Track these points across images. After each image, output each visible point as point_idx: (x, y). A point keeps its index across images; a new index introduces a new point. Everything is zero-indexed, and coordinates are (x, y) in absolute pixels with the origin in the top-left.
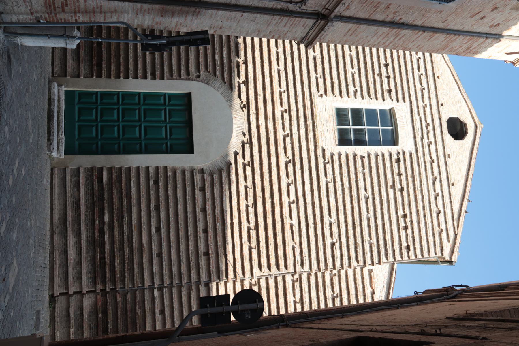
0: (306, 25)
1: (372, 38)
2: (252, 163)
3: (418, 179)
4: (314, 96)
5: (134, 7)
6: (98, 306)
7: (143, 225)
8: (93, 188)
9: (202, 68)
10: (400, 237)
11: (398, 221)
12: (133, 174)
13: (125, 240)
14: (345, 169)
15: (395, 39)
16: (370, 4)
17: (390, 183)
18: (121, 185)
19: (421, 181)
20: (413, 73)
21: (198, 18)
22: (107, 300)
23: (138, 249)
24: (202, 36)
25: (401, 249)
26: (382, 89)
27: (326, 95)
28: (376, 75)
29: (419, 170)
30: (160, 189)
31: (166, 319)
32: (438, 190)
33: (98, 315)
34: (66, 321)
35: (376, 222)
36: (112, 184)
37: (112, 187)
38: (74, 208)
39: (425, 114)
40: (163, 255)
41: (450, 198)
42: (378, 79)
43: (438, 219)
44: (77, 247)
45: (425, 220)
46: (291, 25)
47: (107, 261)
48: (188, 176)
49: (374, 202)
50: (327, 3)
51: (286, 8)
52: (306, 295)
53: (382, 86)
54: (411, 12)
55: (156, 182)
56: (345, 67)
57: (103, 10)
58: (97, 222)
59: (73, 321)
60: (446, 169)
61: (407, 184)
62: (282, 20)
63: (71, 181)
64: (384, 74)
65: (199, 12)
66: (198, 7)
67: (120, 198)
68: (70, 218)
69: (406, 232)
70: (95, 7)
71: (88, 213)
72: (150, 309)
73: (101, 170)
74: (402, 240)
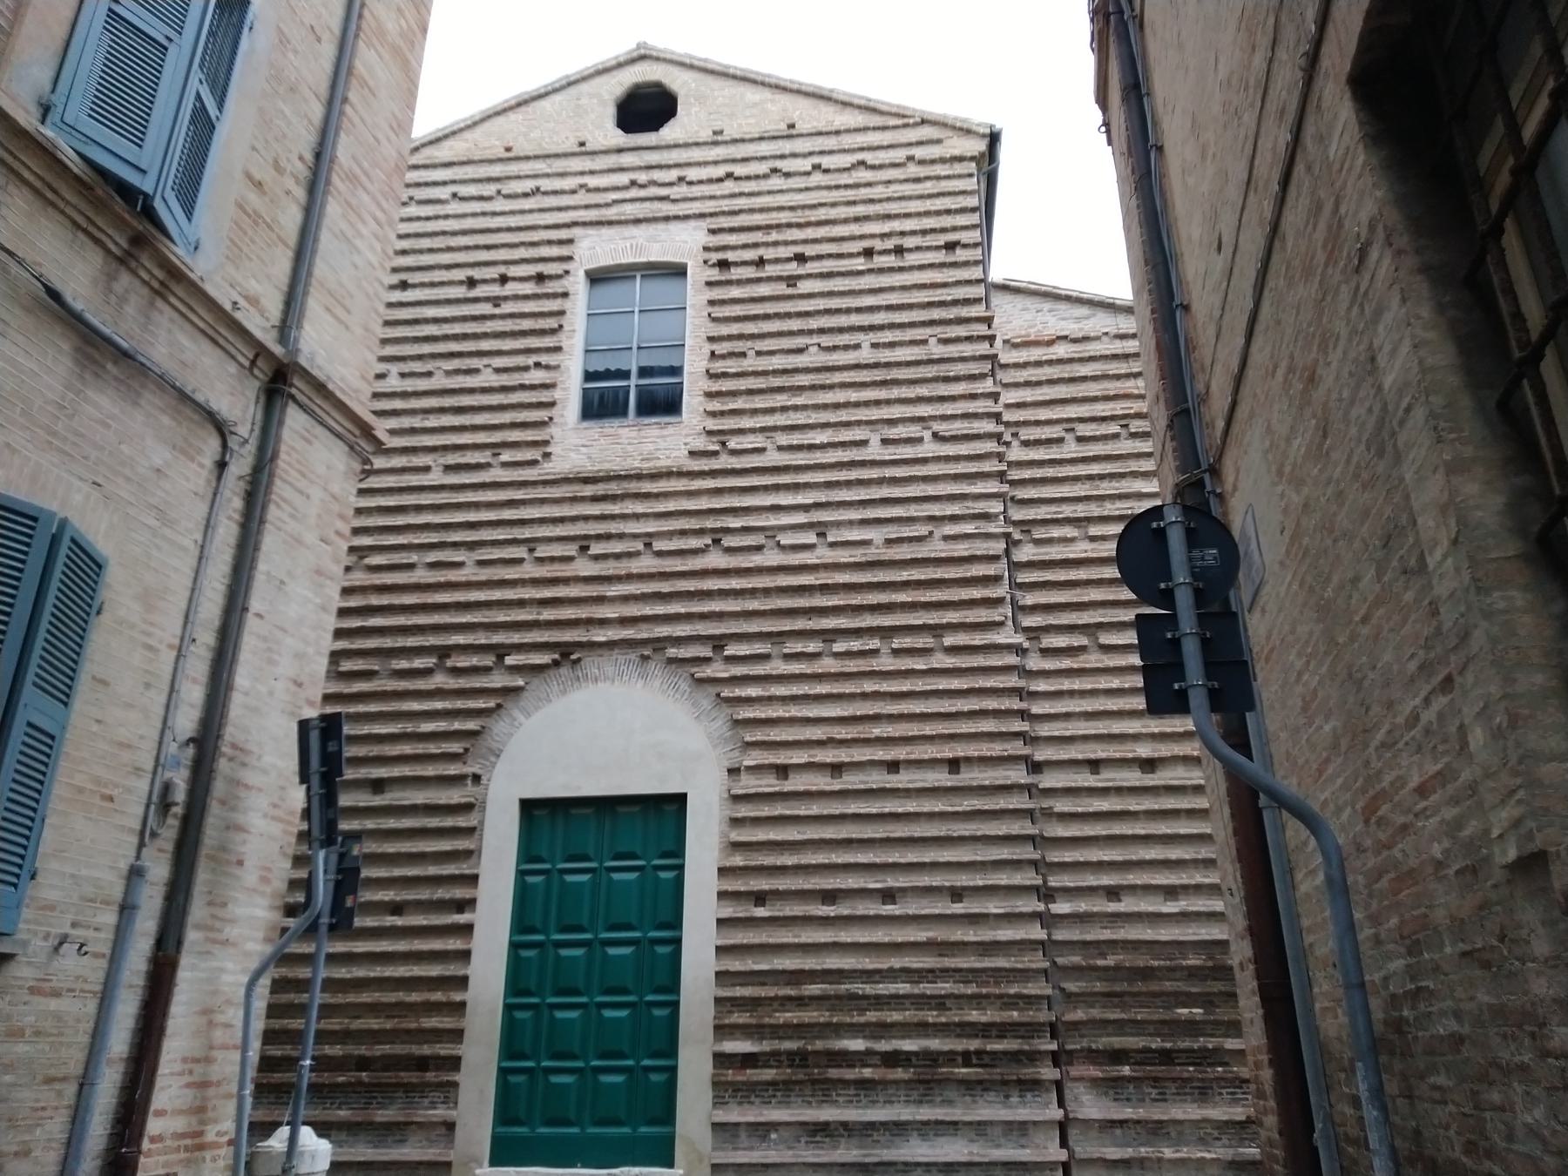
0: (306, 434)
1: (359, 252)
2: (718, 643)
3: (774, 215)
4: (547, 474)
5: (200, 953)
6: (1100, 1075)
7: (874, 939)
8: (773, 1084)
9: (453, 769)
10: (921, 267)
11: (881, 271)
12: (736, 965)
13: (916, 991)
14: (739, 404)
15: (365, 189)
16: (245, 233)
17: (781, 289)
18: (766, 998)
19: (781, 209)
20: (494, 214)
21: (255, 749)
22: (1082, 1050)
23: (941, 955)
24: (314, 736)
25: (954, 265)
26: (536, 297)
27: (546, 443)
28: (497, 311)
29: (752, 211)
30: (781, 888)
31: (1132, 882)
32: (806, 165)
33: (1123, 1078)
34: (1142, 1169)
35: (881, 328)
36: (762, 1026)
37: (771, 1026)
38: (827, 1140)
39: (606, 190)
40: (959, 884)
41: (828, 133)
42: (508, 308)
43: (881, 167)
44: (936, 1135)
45: (880, 201)
46: (303, 475)
47: (973, 1045)
48: (745, 811)
49: (831, 331)
50: (233, 357)
51: (242, 484)
52: (1067, 511)
53: (526, 297)
54: (278, 122)
55: (760, 898)
56: (471, 391)
57: (197, 1054)
58: (867, 1072)
59: (1142, 1150)
60: (752, 140)
61: (786, 243)
62: (285, 500)
63: (751, 1148)
64: (495, 290)
65: (234, 746)
66: (216, 748)
67: (801, 1002)
68: (855, 1152)
69: (910, 250)
70: (187, 1079)
71: (841, 1099)
72: (1106, 928)
73: (721, 1059)
74: (930, 261)
